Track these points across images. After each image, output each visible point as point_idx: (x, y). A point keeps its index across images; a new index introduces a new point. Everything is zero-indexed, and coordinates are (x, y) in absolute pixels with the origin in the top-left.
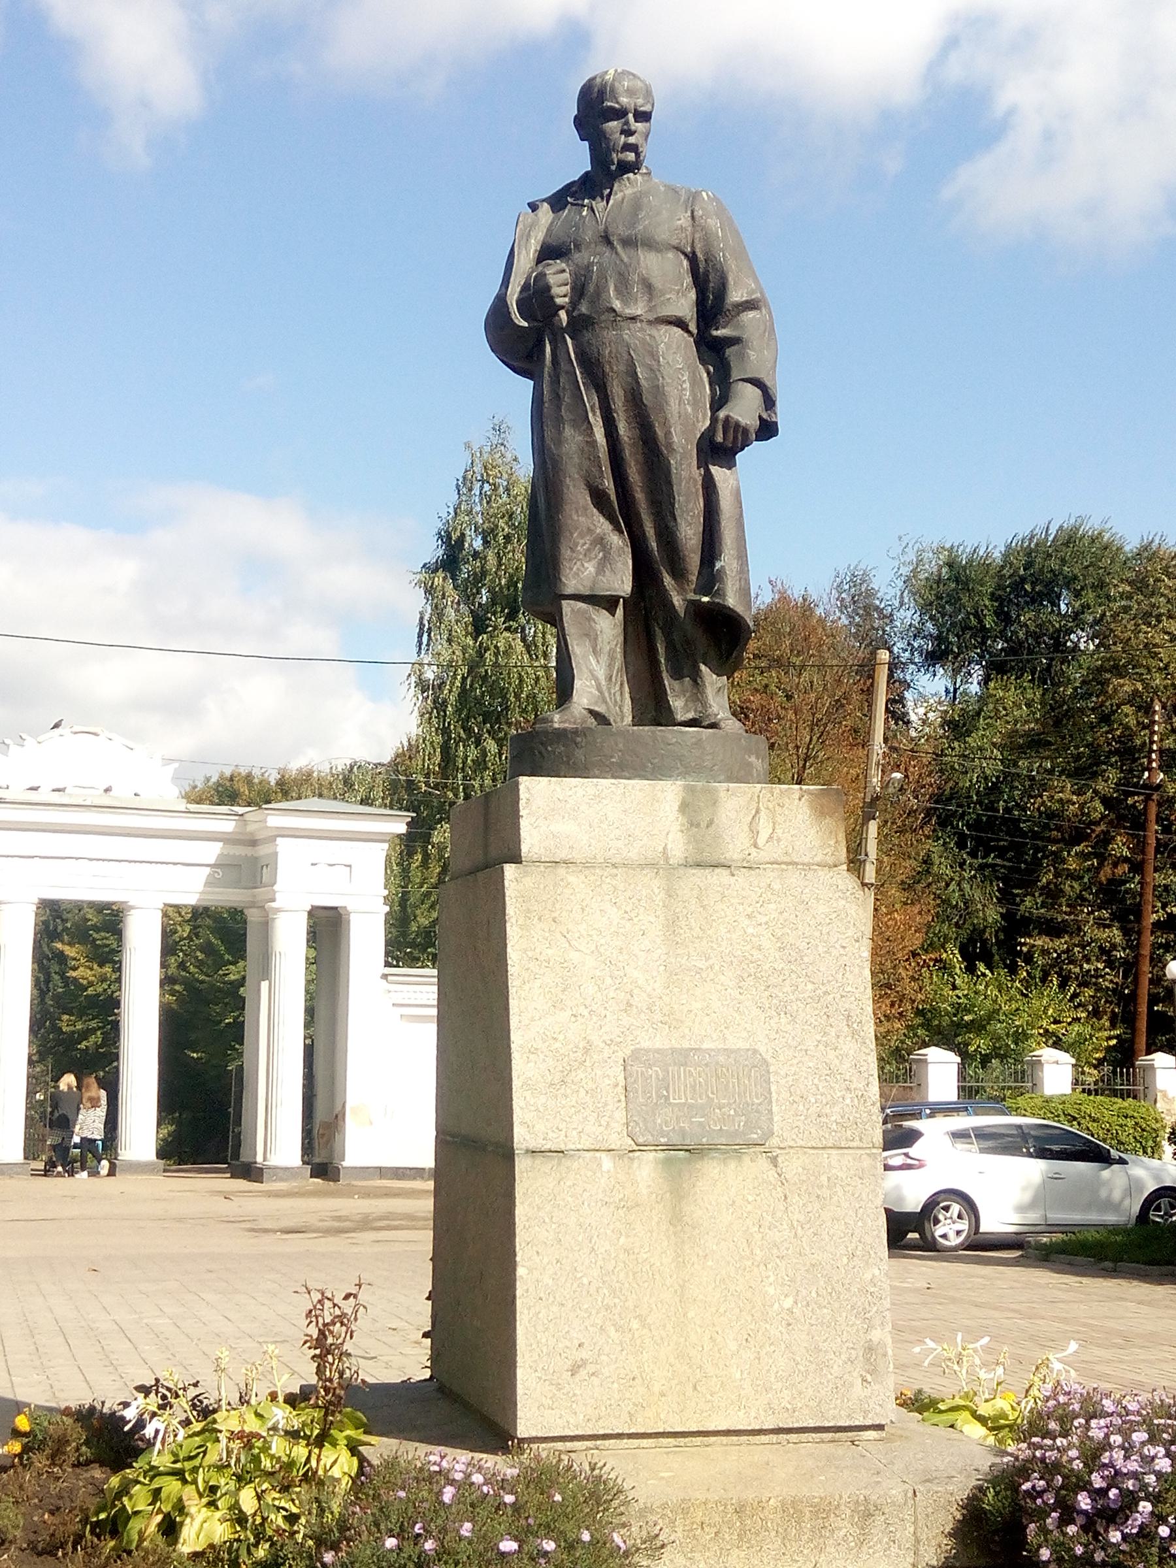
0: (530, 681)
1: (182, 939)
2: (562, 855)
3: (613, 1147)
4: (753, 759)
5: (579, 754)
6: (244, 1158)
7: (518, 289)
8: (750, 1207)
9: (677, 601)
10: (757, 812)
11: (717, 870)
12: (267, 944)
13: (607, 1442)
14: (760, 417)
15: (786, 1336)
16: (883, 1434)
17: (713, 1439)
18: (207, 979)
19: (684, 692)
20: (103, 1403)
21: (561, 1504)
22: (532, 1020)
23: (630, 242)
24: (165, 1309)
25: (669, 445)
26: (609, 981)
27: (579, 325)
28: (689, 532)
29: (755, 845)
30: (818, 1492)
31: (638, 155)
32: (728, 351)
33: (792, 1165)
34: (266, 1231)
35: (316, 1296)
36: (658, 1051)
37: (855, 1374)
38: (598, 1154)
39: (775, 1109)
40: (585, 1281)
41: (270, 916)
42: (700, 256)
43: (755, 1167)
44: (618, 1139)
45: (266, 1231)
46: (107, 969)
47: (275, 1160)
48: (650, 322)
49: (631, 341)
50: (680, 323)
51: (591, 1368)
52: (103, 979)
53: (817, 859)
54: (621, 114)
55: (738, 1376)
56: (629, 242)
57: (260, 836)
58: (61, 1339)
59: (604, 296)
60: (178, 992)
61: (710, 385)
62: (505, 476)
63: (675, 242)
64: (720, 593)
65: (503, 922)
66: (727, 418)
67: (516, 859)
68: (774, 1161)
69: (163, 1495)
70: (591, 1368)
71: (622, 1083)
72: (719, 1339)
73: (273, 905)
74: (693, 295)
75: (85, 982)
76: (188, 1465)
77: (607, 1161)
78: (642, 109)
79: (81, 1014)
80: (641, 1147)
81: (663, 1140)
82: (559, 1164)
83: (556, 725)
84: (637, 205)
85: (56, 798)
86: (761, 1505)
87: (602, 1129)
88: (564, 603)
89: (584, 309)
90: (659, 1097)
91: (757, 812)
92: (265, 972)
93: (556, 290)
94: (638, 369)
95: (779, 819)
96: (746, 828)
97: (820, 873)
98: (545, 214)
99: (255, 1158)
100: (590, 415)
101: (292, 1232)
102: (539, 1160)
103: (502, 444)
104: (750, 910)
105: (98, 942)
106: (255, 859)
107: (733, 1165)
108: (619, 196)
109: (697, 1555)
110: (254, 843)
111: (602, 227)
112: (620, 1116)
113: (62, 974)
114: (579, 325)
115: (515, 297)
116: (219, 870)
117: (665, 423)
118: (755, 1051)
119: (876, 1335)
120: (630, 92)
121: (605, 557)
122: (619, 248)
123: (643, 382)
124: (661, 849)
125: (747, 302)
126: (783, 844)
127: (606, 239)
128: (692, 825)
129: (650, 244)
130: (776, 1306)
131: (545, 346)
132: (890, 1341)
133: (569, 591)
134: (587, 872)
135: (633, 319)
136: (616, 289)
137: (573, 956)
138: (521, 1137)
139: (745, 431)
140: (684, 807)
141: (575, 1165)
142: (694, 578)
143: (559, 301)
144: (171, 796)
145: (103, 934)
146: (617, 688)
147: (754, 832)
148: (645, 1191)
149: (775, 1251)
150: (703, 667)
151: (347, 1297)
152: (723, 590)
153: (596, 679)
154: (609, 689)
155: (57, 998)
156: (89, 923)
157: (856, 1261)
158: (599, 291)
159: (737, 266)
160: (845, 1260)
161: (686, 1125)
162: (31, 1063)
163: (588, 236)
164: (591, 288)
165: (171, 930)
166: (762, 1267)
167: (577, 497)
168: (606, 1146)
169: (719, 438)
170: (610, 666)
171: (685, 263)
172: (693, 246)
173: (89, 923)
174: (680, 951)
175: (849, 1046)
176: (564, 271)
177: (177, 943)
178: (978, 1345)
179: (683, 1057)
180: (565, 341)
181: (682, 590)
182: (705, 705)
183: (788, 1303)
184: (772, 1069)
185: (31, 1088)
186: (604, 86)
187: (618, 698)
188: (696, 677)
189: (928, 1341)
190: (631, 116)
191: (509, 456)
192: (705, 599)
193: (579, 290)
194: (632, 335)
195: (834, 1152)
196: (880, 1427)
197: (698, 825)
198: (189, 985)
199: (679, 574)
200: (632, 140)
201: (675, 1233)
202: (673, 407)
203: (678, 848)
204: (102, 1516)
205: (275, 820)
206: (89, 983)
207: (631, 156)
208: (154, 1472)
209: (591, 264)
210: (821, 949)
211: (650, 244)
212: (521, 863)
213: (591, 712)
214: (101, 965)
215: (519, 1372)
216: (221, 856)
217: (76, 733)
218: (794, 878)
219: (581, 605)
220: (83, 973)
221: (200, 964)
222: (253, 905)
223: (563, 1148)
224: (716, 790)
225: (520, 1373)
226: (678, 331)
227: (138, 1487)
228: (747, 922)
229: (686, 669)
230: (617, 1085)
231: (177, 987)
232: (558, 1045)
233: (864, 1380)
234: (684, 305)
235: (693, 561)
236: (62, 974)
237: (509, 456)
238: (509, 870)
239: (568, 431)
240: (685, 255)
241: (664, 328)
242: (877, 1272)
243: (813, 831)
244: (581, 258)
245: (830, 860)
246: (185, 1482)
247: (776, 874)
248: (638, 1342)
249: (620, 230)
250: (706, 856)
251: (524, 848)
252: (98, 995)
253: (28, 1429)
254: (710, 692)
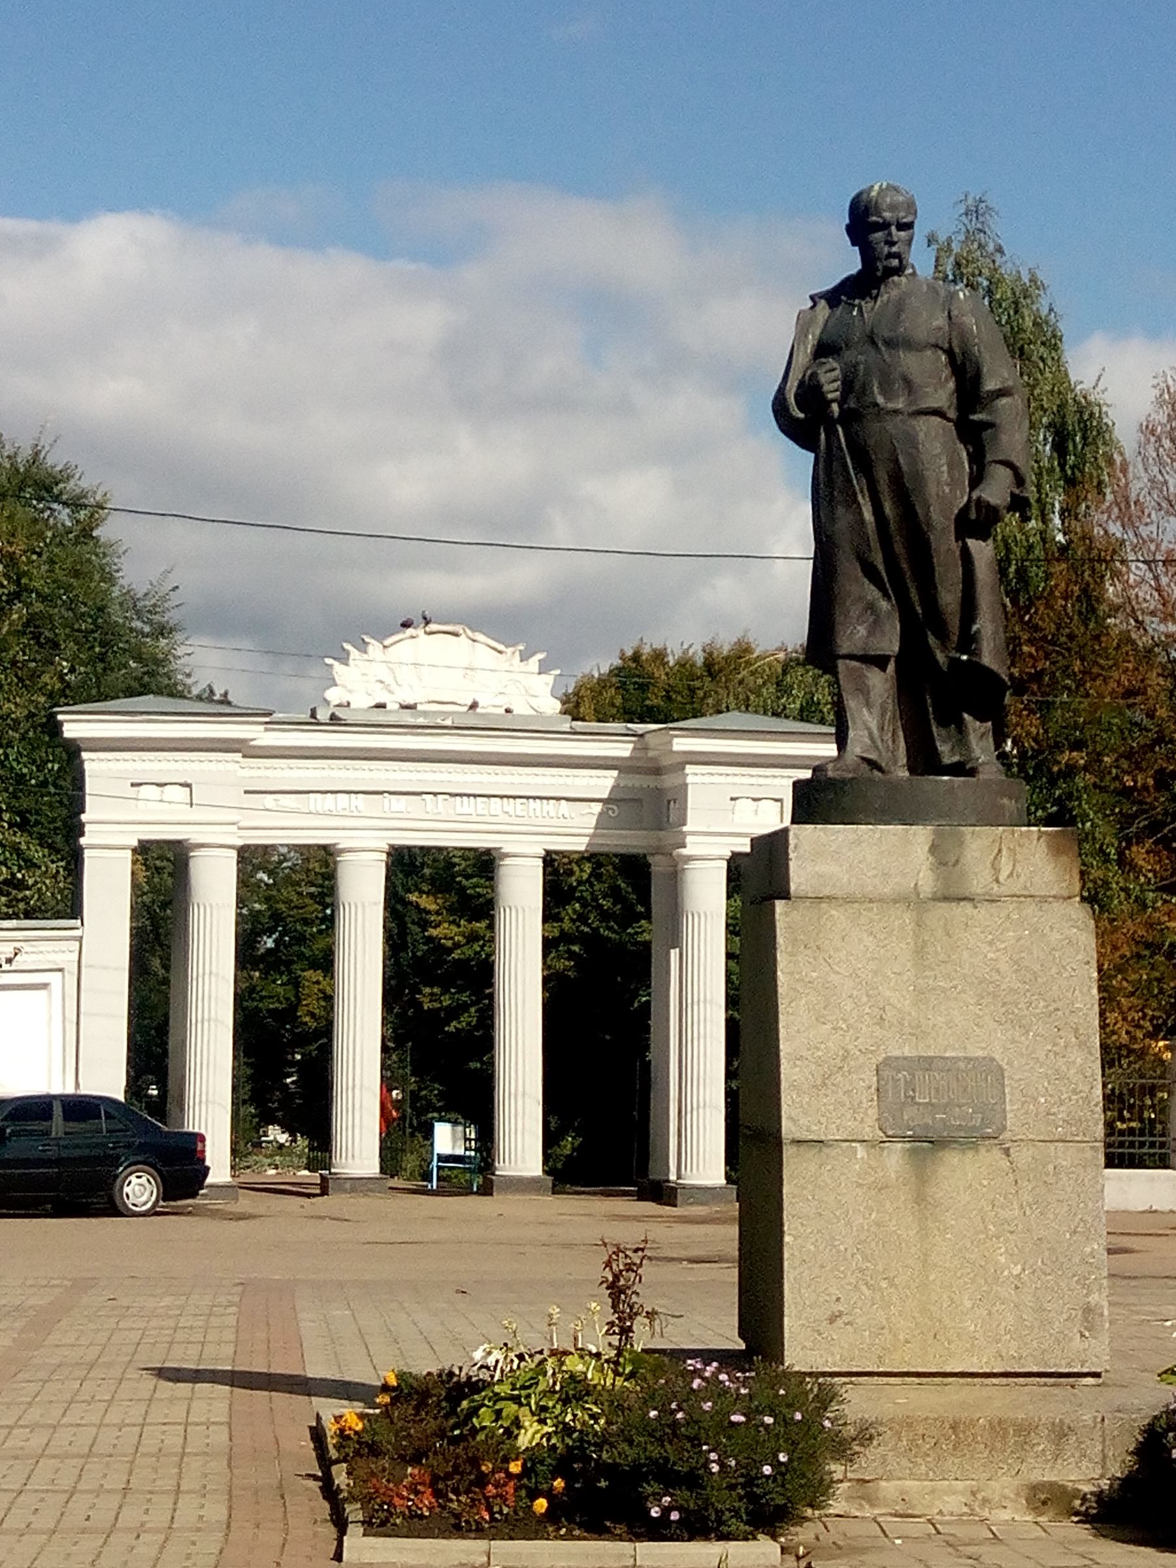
1: (580, 883)
2: (826, 891)
3: (866, 1138)
4: (1005, 801)
9: (940, 657)
11: (962, 903)
12: (676, 898)
13: (860, 1379)
14: (1012, 494)
16: (1100, 1381)
17: (950, 1380)
18: (613, 936)
19: (950, 738)
20: (461, 1369)
22: (798, 1031)
24: (535, 1325)
25: (929, 524)
26: (865, 999)
27: (850, 418)
28: (949, 598)
29: (997, 881)
30: (1021, 1416)
31: (901, 262)
33: (1023, 1156)
34: (672, 1259)
35: (611, 1250)
37: (1075, 1330)
38: (854, 1144)
40: (842, 1248)
41: (679, 868)
42: (957, 350)
43: (990, 1157)
44: (870, 1131)
45: (672, 1259)
46: (481, 925)
47: (694, 1178)
49: (893, 432)
50: (938, 413)
51: (845, 1319)
52: (473, 937)
53: (1053, 893)
54: (885, 226)
56: (890, 343)
57: (665, 762)
63: (933, 341)
65: (774, 948)
66: (979, 499)
67: (785, 895)
68: (1007, 1152)
69: (504, 1414)
71: (874, 1086)
73: (684, 851)
75: (449, 943)
76: (523, 1393)
77: (861, 1151)
78: (905, 220)
80: (891, 1139)
81: (910, 1133)
82: (820, 1151)
84: (900, 307)
85: (408, 718)
86: (973, 1423)
87: (856, 1123)
88: (840, 663)
89: (852, 404)
91: (1000, 851)
92: (675, 938)
93: (826, 388)
95: (1018, 857)
96: (989, 865)
97: (1055, 904)
102: (803, 1148)
103: (980, 231)
106: (659, 792)
107: (970, 1154)
108: (885, 297)
109: (919, 1460)
110: (657, 771)
111: (869, 329)
112: (873, 1113)
114: (850, 418)
116: (615, 808)
118: (993, 1060)
119: (1094, 1298)
120: (893, 207)
121: (875, 622)
122: (883, 349)
123: (905, 468)
124: (912, 885)
125: (1000, 390)
127: (871, 340)
128: (940, 863)
129: (909, 345)
130: (1006, 1273)
131: (819, 434)
132: (1105, 1304)
133: (843, 651)
134: (847, 906)
135: (896, 412)
138: (788, 1128)
140: (933, 849)
142: (955, 639)
143: (830, 396)
146: (890, 735)
147: (996, 869)
148: (893, 1176)
149: (1006, 1226)
152: (980, 650)
153: (868, 729)
154: (881, 737)
158: (865, 389)
159: (991, 357)
160: (1068, 1236)
163: (857, 335)
164: (857, 386)
168: (860, 1138)
170: (883, 715)
172: (950, 343)
173: (457, 868)
174: (927, 973)
175: (1077, 1056)
176: (834, 370)
181: (944, 647)
182: (969, 749)
183: (1017, 1270)
188: (961, 727)
190: (893, 228)
191: (991, 247)
193: (848, 385)
194: (892, 426)
195: (1061, 1144)
196: (1096, 1375)
197: (945, 864)
198: (592, 941)
199: (943, 635)
200: (894, 249)
201: (919, 1211)
202: (932, 489)
203: (927, 882)
204: (457, 1432)
206: (454, 944)
211: (909, 345)
212: (789, 899)
213: (864, 759)
216: (614, 788)
218: (1030, 909)
220: (445, 931)
221: (605, 916)
222: (658, 851)
223: (823, 1138)
224: (962, 834)
225: (789, 1323)
226: (936, 420)
230: (870, 1087)
231: (576, 948)
232: (820, 1053)
233: (1082, 1336)
234: (943, 395)
235: (954, 624)
237: (991, 247)
238: (779, 905)
239: (840, 510)
242: (1096, 1247)
243: (1050, 868)
244: (849, 356)
245: (1066, 894)
247: (1015, 905)
248: (887, 1298)
250: (954, 891)
251: (793, 887)
252: (469, 960)
254: (973, 739)
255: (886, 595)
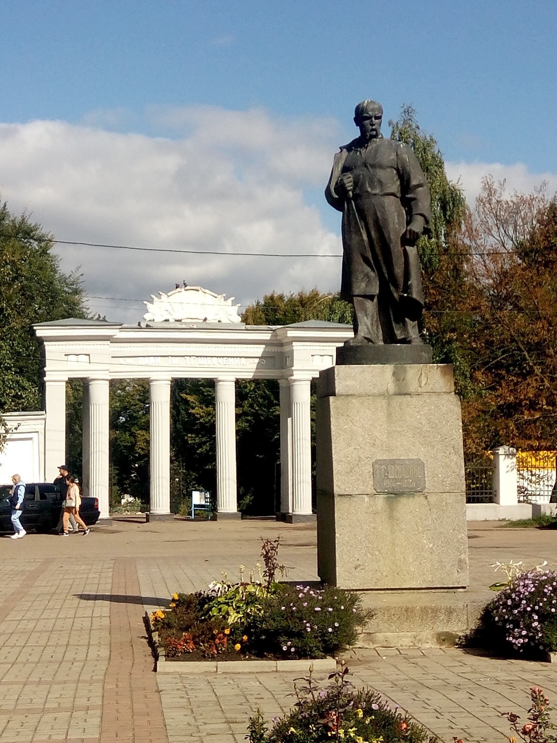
0: (428, 252)
1: (250, 391)
2: (350, 393)
5: (358, 355)
6: (283, 511)
7: (334, 184)
8: (417, 513)
9: (396, 295)
10: (421, 374)
11: (406, 396)
14: (424, 228)
15: (430, 557)
16: (466, 590)
20: (204, 592)
21: (337, 600)
23: (373, 166)
25: (390, 239)
26: (367, 436)
27: (356, 197)
28: (399, 270)
29: (421, 387)
32: (412, 203)
33: (433, 499)
34: (290, 545)
35: (265, 541)
36: (384, 460)
39: (426, 479)
40: (359, 538)
43: (419, 499)
45: (290, 545)
48: (382, 195)
53: (444, 391)
54: (370, 118)
55: (413, 570)
57: (285, 341)
58: (190, 583)
59: (364, 187)
60: (250, 420)
61: (407, 215)
62: (412, 136)
63: (390, 165)
64: (410, 293)
67: (334, 394)
68: (426, 497)
69: (222, 610)
70: (362, 567)
71: (372, 471)
72: (406, 558)
74: (398, 183)
75: (199, 416)
76: (230, 601)
77: (366, 499)
79: (197, 433)
80: (379, 493)
81: (386, 491)
83: (351, 344)
84: (376, 151)
85: (178, 325)
89: (358, 191)
90: (385, 476)
91: (421, 374)
92: (290, 414)
94: (378, 213)
96: (417, 380)
98: (345, 152)
99: (288, 510)
100: (361, 229)
101: (303, 546)
102: (343, 498)
104: (418, 410)
105: (205, 394)
107: (411, 499)
110: (281, 345)
111: (364, 161)
112: (371, 483)
113: (186, 410)
115: (333, 187)
117: (389, 232)
118: (419, 460)
119: (463, 556)
120: (373, 110)
123: (380, 217)
126: (430, 386)
129: (381, 167)
133: (356, 293)
135: (375, 194)
136: (369, 184)
137: (354, 427)
139: (417, 234)
140: (394, 374)
141: (356, 500)
142: (401, 287)
143: (349, 188)
144: (238, 319)
145: (208, 389)
147: (420, 381)
148: (380, 508)
150: (407, 319)
151: (275, 541)
153: (366, 325)
154: (372, 328)
155: (184, 423)
156: (200, 383)
157: (456, 531)
158: (363, 184)
161: (395, 485)
162: (172, 462)
163: (359, 163)
164: (360, 184)
165: (244, 386)
166: (422, 534)
167: (358, 259)
169: (408, 237)
170: (372, 320)
171: (395, 172)
173: (200, 383)
175: (454, 458)
176: (350, 177)
177: (248, 393)
178: (517, 564)
179: (393, 462)
180: (351, 203)
181: (397, 291)
182: (408, 333)
183: (431, 546)
184: (425, 466)
185: (172, 476)
186: (363, 108)
187: (376, 331)
188: (404, 323)
189: (497, 562)
190: (373, 119)
192: (406, 295)
196: (464, 588)
198: (256, 416)
199: (396, 286)
200: (374, 127)
202: (391, 226)
204: (203, 618)
205: (291, 333)
207: (374, 133)
208: (219, 603)
209: (360, 175)
210: (444, 423)
211: (381, 167)
212: (335, 395)
213: (365, 338)
214: (207, 406)
215: (337, 568)
217: (187, 290)
218: (434, 398)
219: (360, 298)
220: (197, 411)
221: (260, 405)
223: (351, 494)
224: (405, 367)
226: (392, 197)
227: (214, 608)
228: (417, 414)
229: (401, 321)
233: (458, 571)
234: (395, 187)
235: (401, 281)
236: (186, 410)
238: (331, 399)
239: (353, 236)
240: (395, 169)
241: (387, 197)
243: (442, 381)
244: (357, 172)
245: (448, 391)
246: (229, 606)
249: (370, 161)
251: (337, 391)
253: (177, 599)
254: (409, 328)
255: (373, 270)
